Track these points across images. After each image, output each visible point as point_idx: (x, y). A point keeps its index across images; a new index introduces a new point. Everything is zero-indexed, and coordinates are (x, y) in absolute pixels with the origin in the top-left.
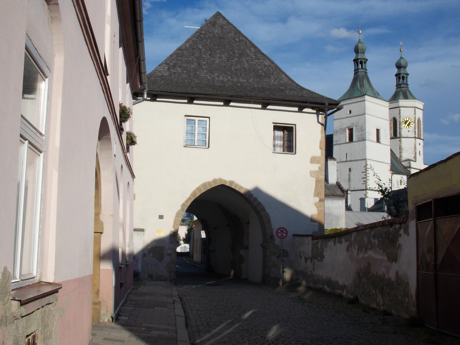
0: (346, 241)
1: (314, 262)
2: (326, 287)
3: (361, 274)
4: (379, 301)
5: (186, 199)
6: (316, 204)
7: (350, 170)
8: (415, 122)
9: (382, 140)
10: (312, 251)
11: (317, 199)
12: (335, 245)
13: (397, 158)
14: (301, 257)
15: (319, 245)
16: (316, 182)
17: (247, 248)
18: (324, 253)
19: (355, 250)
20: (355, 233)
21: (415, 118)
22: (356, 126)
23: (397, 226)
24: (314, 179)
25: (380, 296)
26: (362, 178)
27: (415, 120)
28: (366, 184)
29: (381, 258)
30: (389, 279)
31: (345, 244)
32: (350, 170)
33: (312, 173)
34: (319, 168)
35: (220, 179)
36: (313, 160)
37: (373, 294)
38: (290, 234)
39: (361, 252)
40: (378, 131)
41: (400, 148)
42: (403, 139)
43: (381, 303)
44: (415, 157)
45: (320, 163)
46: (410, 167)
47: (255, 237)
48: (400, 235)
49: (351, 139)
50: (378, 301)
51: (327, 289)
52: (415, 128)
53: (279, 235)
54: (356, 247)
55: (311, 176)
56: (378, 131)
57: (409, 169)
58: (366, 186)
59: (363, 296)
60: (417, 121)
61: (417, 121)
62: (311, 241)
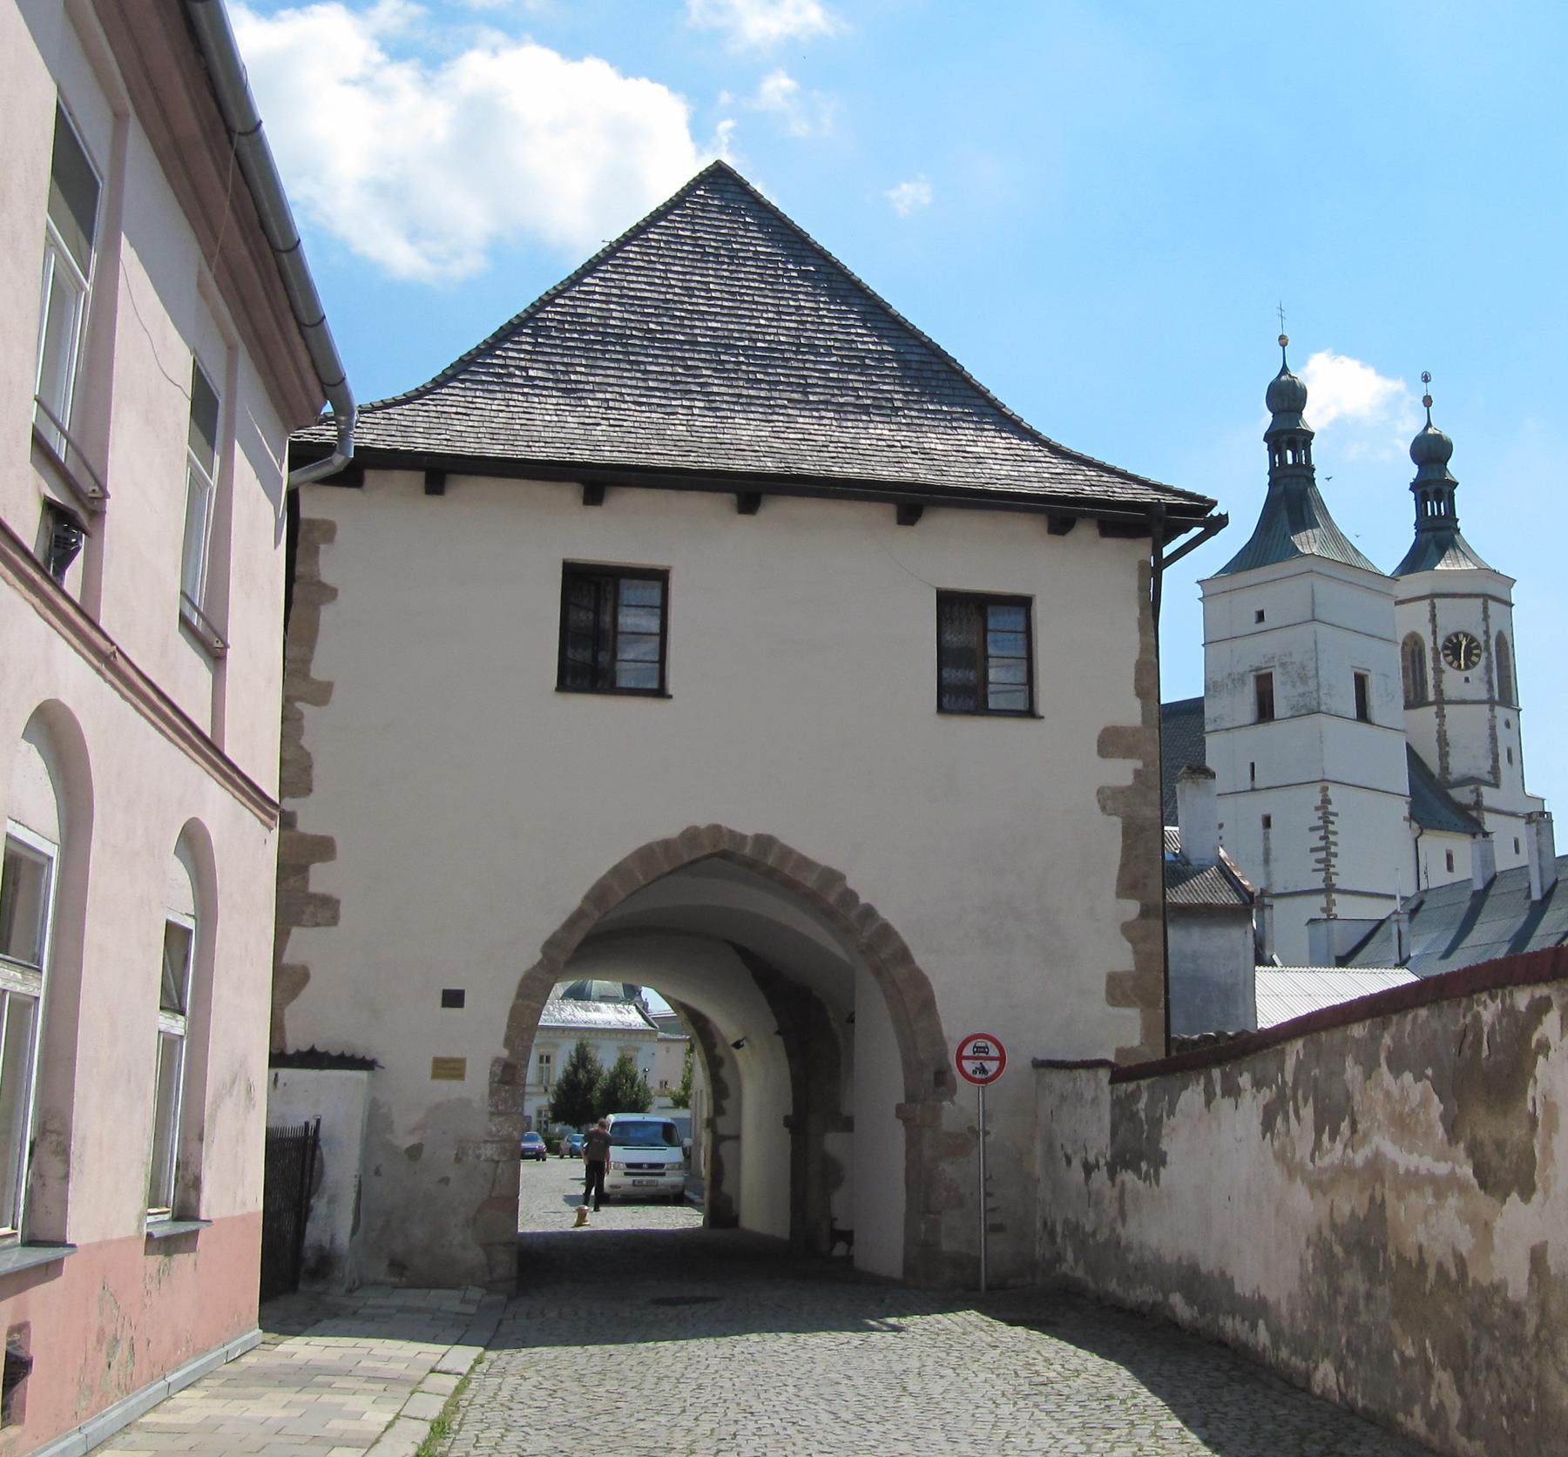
0: (1258, 1084)
1: (1123, 1184)
2: (1176, 1299)
3: (1338, 1250)
4: (1441, 1405)
5: (564, 918)
6: (1126, 929)
7: (1267, 822)
8: (1487, 648)
9: (1375, 712)
10: (1114, 1134)
11: (1132, 908)
12: (1208, 1103)
13: (1432, 776)
14: (1069, 1162)
15: (1141, 1105)
16: (1126, 833)
17: (848, 1125)
18: (1164, 1145)
19: (1301, 1127)
20: (1299, 1044)
21: (1486, 632)
22: (1283, 665)
23: (1522, 999)
24: (1117, 821)
25: (1443, 1377)
26: (1313, 850)
27: (1487, 642)
28: (1327, 869)
29: (1442, 1169)
30: (1498, 1288)
31: (1252, 1105)
32: (1267, 822)
33: (1108, 799)
34: (1137, 773)
35: (716, 830)
36: (1112, 742)
37: (1406, 1362)
38: (1018, 1061)
39: (1333, 1138)
40: (1360, 682)
41: (1443, 740)
42: (1448, 709)
43: (1455, 1417)
44: (1495, 770)
45: (1140, 757)
46: (1478, 805)
47: (879, 1071)
48: (1544, 1047)
49: (1265, 711)
50: (1433, 1401)
51: (1179, 1305)
52: (1488, 669)
53: (969, 1066)
54: (1308, 1112)
55: (1103, 808)
56: (1360, 682)
57: (1474, 814)
58: (1328, 879)
59: (1351, 1364)
60: (1493, 642)
61: (1493, 642)
62: (1106, 1088)
